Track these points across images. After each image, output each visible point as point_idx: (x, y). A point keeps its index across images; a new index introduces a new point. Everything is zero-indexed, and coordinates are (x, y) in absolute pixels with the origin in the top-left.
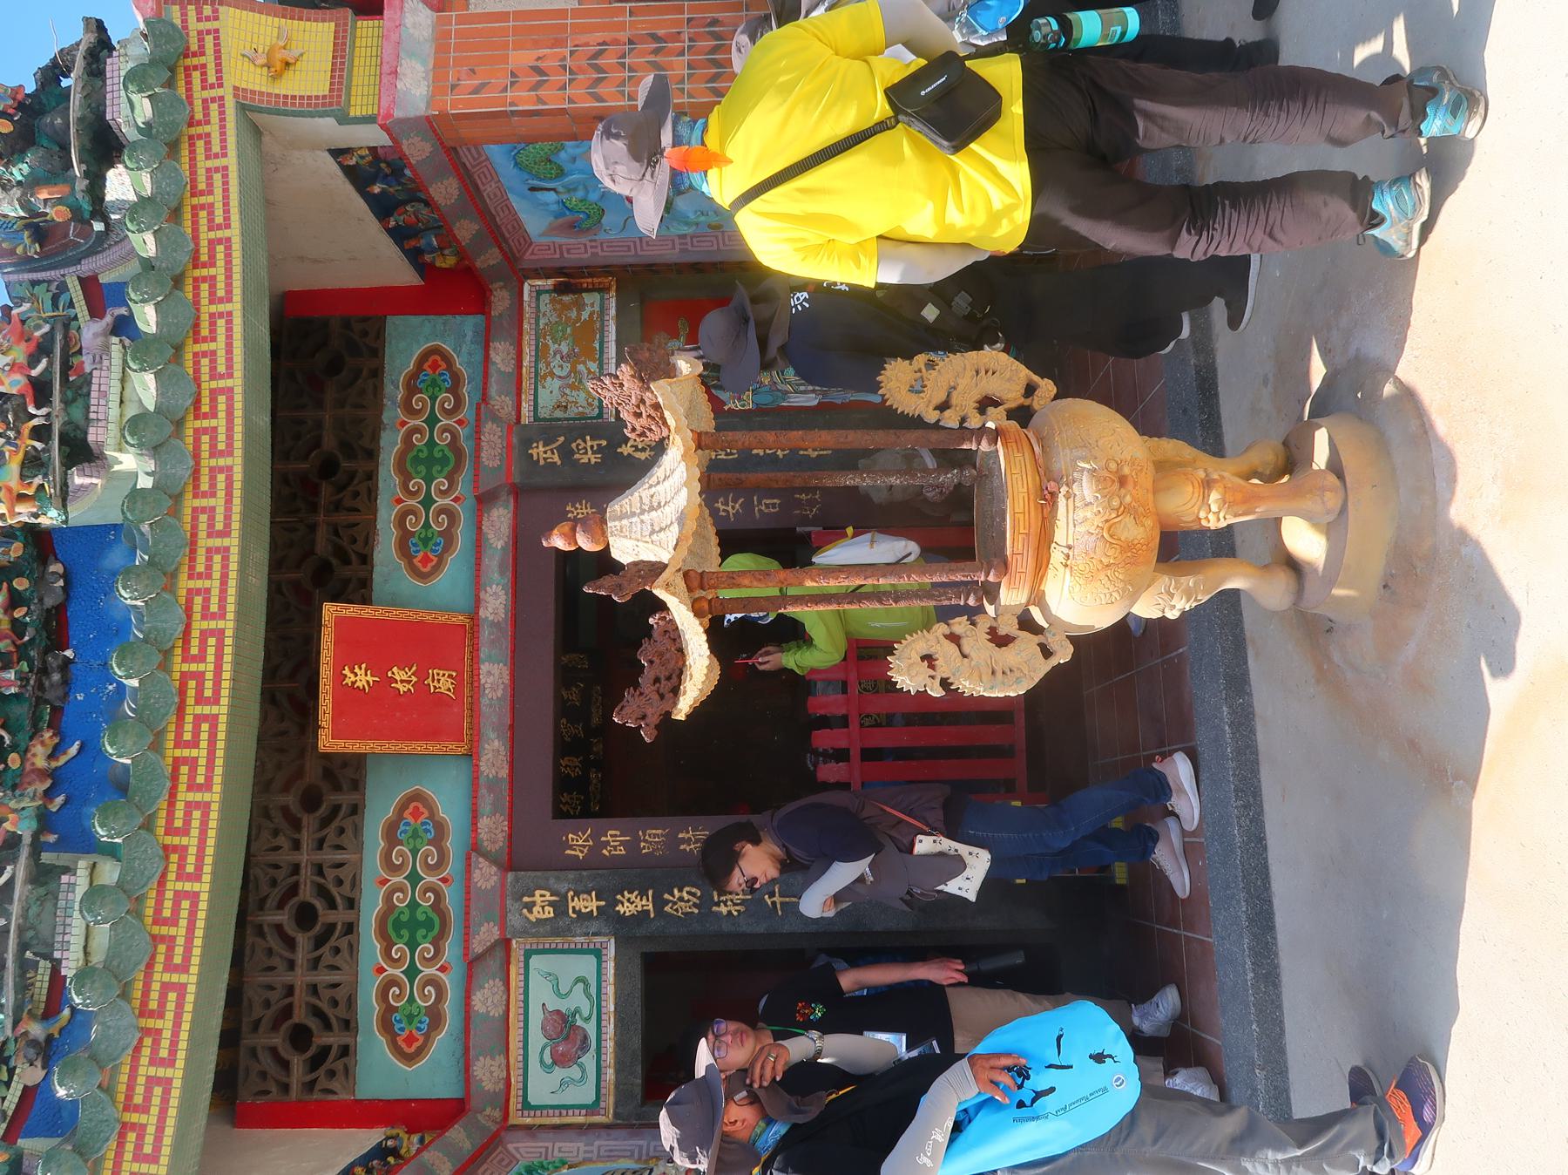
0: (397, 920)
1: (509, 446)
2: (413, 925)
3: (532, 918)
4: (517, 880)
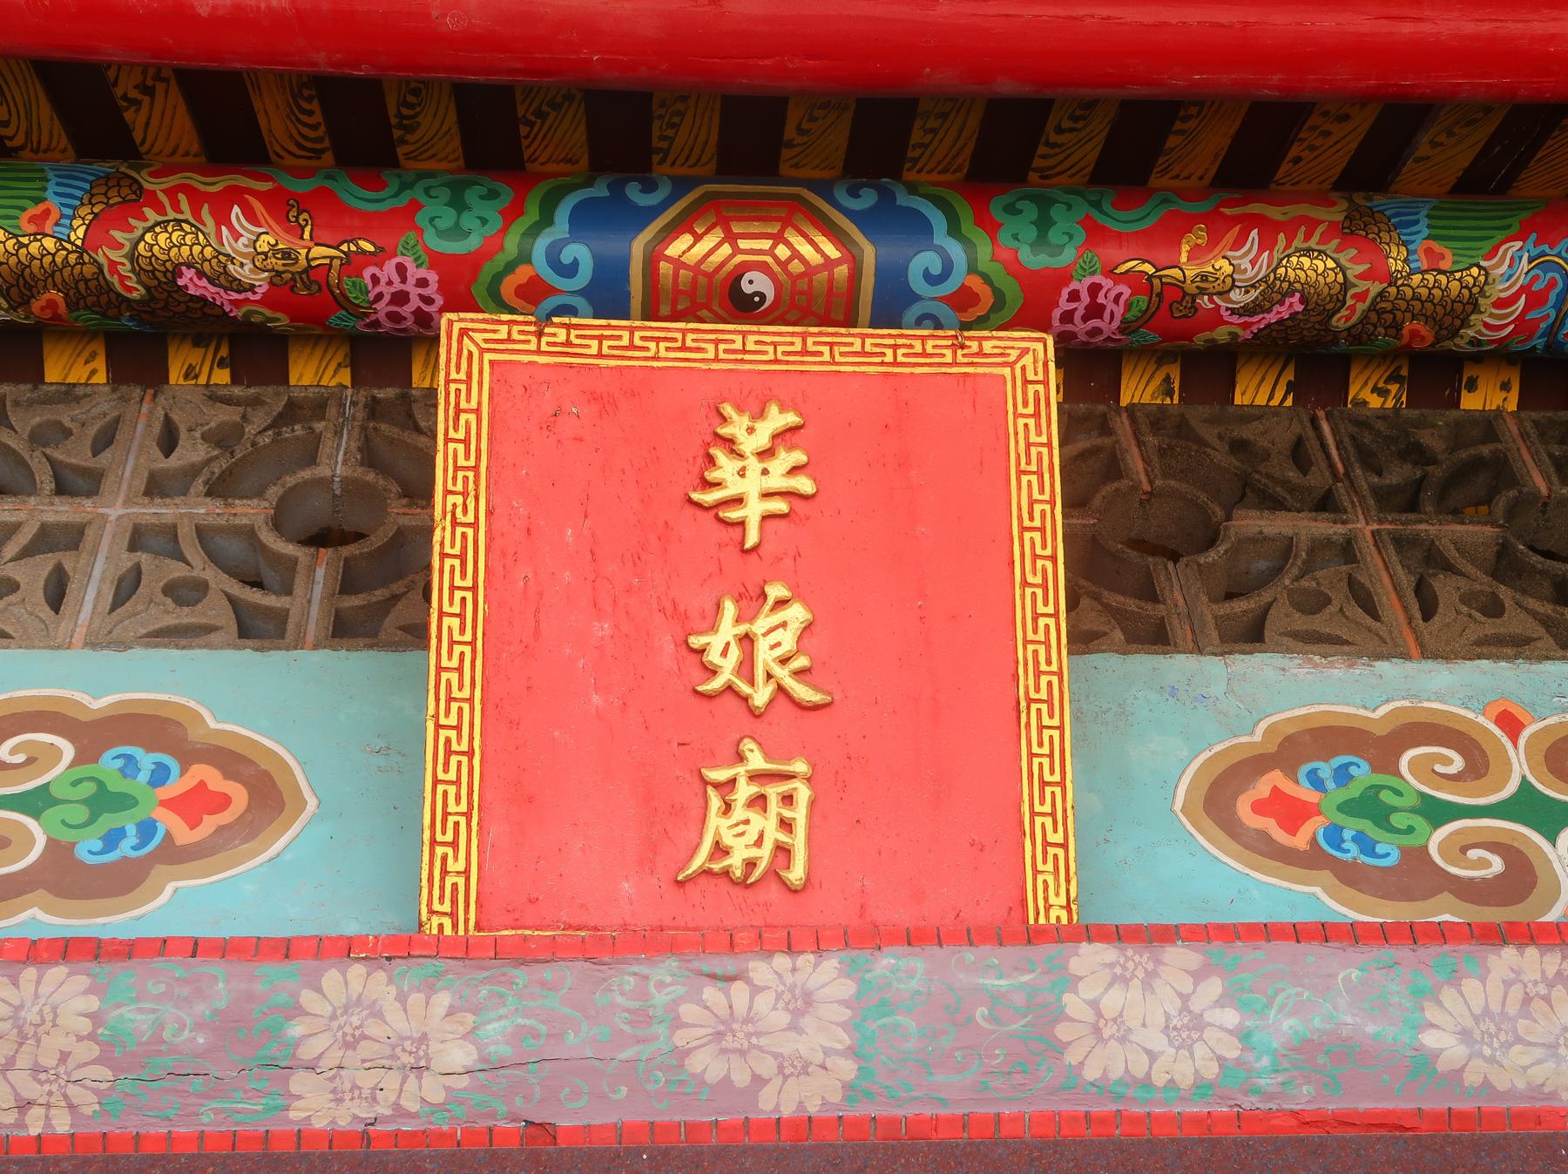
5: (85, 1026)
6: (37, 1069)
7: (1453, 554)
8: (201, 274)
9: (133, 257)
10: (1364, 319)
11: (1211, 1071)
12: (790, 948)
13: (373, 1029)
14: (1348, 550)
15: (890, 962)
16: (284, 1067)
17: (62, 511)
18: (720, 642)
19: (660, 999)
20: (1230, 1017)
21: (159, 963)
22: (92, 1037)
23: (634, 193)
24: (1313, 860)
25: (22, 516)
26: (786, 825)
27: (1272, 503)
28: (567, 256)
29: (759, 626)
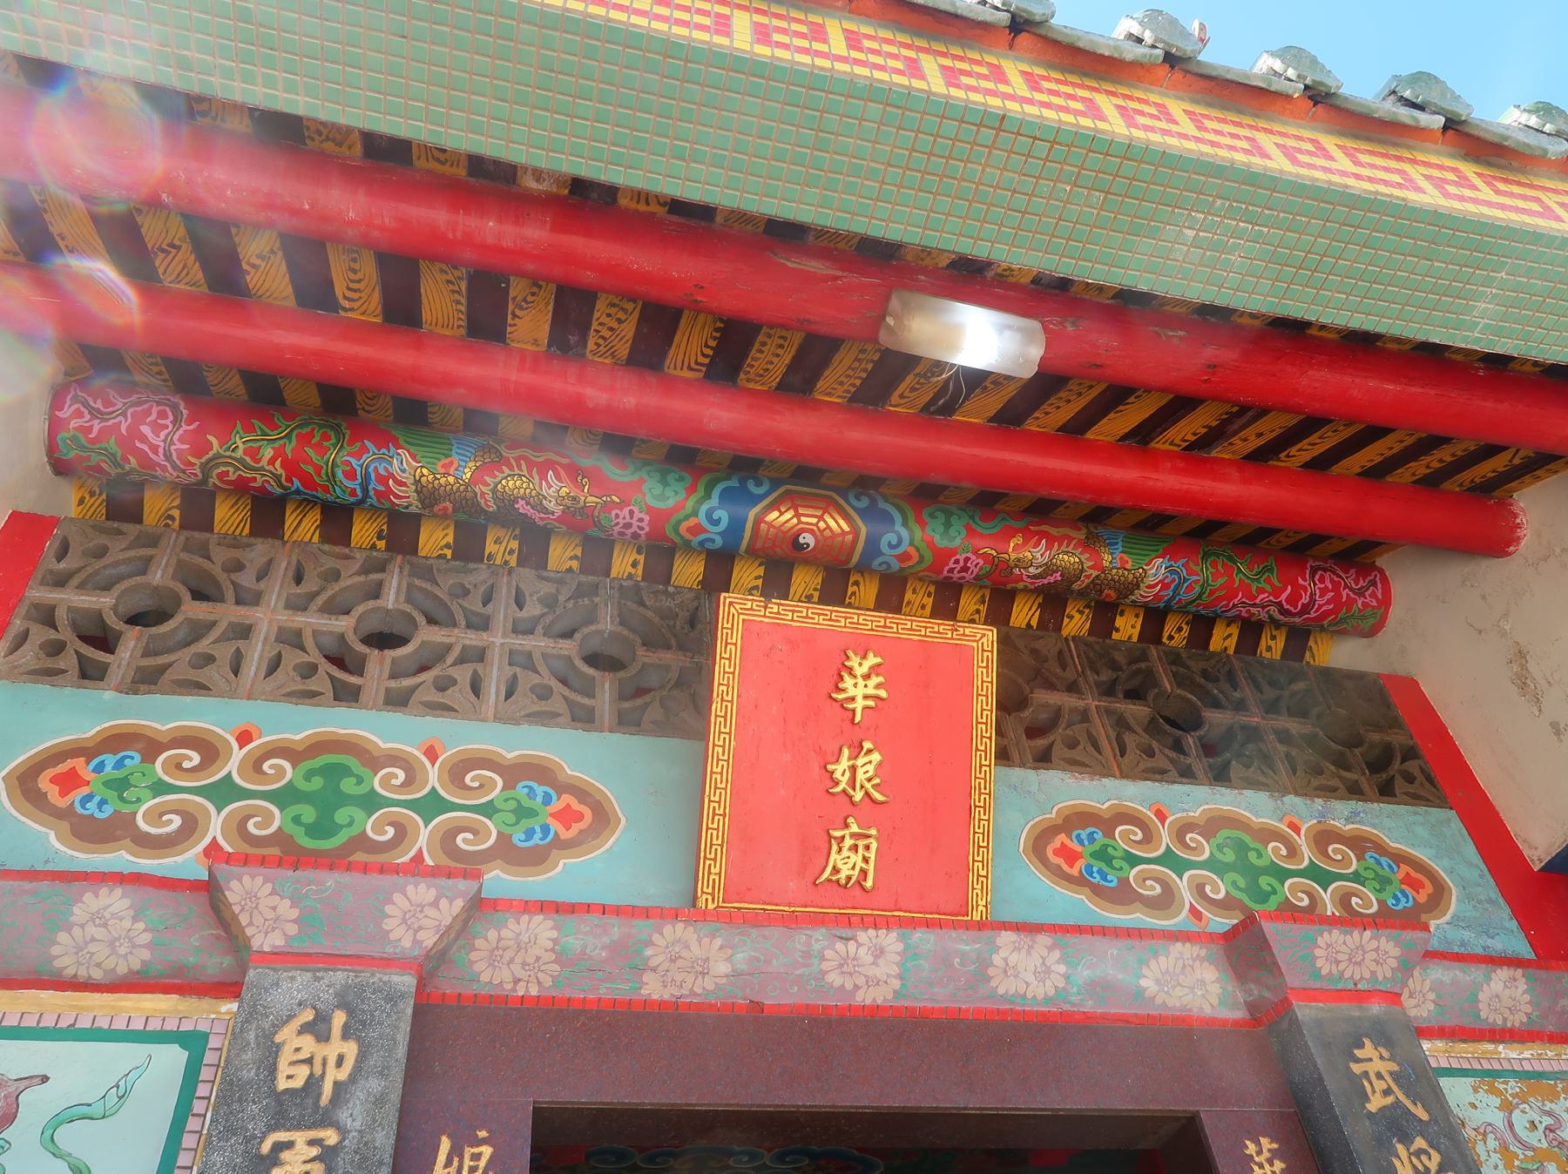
0: (345, 771)
1: (1359, 996)
2: (329, 801)
3: (287, 1034)
4: (392, 998)
5: (550, 945)
6: (524, 964)
7: (1132, 722)
8: (528, 503)
9: (494, 491)
10: (1088, 586)
11: (1052, 992)
12: (876, 926)
13: (685, 954)
14: (1085, 716)
15: (919, 935)
16: (641, 969)
17: (472, 639)
18: (840, 769)
19: (816, 947)
20: (1062, 969)
21: (588, 917)
22: (552, 950)
23: (751, 485)
24: (1079, 882)
25: (452, 640)
26: (866, 860)
27: (1051, 687)
28: (715, 516)
29: (860, 762)
